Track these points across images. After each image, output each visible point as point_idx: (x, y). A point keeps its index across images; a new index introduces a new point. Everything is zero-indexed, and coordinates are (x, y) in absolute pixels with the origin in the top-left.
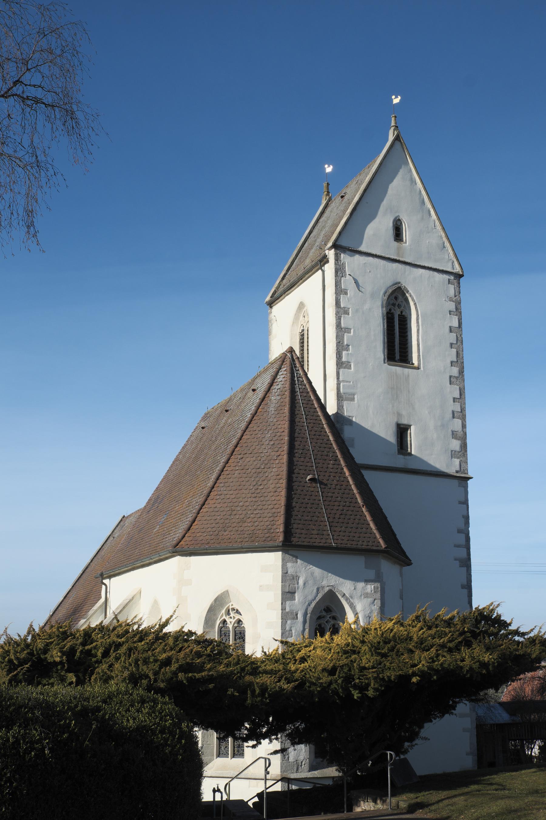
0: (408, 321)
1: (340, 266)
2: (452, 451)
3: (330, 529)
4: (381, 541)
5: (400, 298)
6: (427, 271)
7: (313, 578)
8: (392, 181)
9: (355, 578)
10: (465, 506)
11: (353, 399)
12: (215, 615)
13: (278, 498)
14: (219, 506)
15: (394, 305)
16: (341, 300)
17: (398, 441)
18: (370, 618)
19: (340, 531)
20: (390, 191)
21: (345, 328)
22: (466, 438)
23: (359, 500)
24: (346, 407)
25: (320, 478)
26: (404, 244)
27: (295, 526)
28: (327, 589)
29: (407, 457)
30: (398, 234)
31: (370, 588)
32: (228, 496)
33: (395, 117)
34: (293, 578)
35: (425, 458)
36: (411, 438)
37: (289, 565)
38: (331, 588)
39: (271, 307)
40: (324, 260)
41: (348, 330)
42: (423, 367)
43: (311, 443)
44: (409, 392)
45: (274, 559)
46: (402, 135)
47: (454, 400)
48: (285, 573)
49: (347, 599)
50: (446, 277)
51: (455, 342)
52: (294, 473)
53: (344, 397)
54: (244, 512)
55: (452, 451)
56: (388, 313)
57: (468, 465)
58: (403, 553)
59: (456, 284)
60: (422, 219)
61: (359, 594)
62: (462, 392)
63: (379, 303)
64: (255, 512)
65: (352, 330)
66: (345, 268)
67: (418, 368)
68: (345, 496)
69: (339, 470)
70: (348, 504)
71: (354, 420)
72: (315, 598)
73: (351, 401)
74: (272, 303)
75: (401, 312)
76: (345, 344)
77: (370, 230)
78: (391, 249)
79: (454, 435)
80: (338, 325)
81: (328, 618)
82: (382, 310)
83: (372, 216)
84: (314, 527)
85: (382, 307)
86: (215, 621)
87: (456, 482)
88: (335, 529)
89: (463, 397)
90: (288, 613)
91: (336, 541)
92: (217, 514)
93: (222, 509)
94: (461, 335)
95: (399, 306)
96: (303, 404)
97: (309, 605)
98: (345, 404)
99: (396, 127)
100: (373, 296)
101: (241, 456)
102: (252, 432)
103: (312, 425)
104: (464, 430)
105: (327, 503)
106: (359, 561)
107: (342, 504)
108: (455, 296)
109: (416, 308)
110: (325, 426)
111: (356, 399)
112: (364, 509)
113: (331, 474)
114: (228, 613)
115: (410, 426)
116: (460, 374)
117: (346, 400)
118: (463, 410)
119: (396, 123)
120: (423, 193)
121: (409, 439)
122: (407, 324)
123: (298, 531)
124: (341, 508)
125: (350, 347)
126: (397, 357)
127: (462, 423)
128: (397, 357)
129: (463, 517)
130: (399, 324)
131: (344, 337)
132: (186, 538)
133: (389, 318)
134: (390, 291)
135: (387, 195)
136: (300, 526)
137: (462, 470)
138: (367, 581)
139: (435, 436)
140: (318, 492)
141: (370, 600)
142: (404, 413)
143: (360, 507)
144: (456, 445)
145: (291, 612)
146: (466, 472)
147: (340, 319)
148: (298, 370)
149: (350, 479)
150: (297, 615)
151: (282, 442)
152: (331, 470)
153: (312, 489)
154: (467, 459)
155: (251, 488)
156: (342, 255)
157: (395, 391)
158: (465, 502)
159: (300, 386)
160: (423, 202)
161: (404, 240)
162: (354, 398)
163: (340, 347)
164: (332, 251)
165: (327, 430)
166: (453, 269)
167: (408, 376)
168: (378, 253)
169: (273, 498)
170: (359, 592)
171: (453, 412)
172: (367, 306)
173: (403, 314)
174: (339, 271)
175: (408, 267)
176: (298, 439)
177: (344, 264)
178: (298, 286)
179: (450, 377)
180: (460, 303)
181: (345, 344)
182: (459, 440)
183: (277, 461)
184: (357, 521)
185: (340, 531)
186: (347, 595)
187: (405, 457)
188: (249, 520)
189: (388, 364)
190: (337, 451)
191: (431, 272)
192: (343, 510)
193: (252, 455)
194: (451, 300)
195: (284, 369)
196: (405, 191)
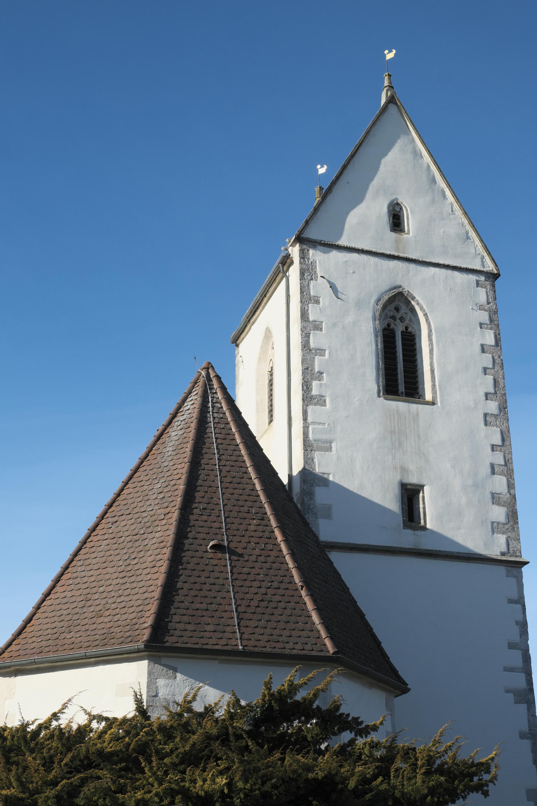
0: (417, 340)
1: (307, 265)
2: (493, 523)
3: (238, 624)
4: (328, 643)
5: (404, 309)
6: (443, 271)
8: (385, 154)
10: (519, 606)
11: (330, 449)
13: (155, 576)
14: (69, 594)
15: (393, 318)
16: (310, 311)
17: (403, 508)
19: (257, 627)
20: (382, 168)
21: (316, 350)
23: (297, 579)
24: (318, 460)
25: (232, 545)
26: (405, 236)
27: (176, 618)
29: (419, 533)
30: (396, 222)
32: (85, 580)
33: (389, 75)
36: (424, 503)
37: (161, 682)
39: (237, 346)
40: (286, 261)
41: (320, 352)
42: (442, 402)
43: (223, 494)
44: (419, 437)
46: (399, 97)
47: (493, 448)
50: (473, 278)
51: (491, 366)
53: (315, 445)
54: (104, 601)
55: (493, 523)
56: (384, 330)
57: (522, 544)
59: (488, 287)
60: (433, 201)
62: (505, 437)
63: (369, 314)
64: (119, 600)
65: (327, 352)
66: (316, 266)
67: (433, 403)
68: (272, 572)
69: (267, 534)
70: (275, 584)
71: (331, 478)
73: (327, 451)
74: (237, 339)
75: (407, 328)
76: (316, 371)
77: (353, 218)
78: (388, 242)
79: (495, 499)
80: (305, 345)
82: (374, 324)
83: (358, 199)
84: (209, 620)
85: (374, 319)
87: (502, 570)
88: (248, 623)
89: (507, 443)
91: (245, 643)
92: (65, 607)
93: (73, 599)
94: (499, 357)
95: (402, 319)
96: (216, 438)
98: (317, 456)
99: (391, 87)
100: (359, 304)
101: (115, 519)
102: (136, 484)
103: (228, 468)
104: (512, 491)
105: (238, 583)
110: (250, 470)
111: (334, 449)
112: (303, 593)
113: (252, 539)
115: (422, 486)
116: (500, 410)
117: (318, 451)
118: (508, 462)
119: (390, 83)
120: (433, 168)
121: (421, 506)
122: (415, 344)
123: (181, 626)
124: (263, 590)
125: (324, 375)
126: (402, 388)
128: (402, 388)
129: (517, 623)
130: (403, 344)
131: (313, 361)
132: (13, 648)
133: (387, 337)
134: (386, 297)
135: (379, 173)
136: (186, 619)
137: (511, 551)
139: (464, 500)
140: (226, 566)
142: (412, 467)
143: (297, 590)
144: (499, 514)
146: (518, 554)
147: (308, 337)
148: (216, 393)
149: (283, 547)
151: (176, 493)
152: (253, 534)
153: (214, 562)
154: (519, 535)
155: (121, 564)
156: (311, 252)
157: (396, 436)
158: (520, 601)
159: (216, 415)
160: (433, 181)
161: (406, 230)
162: (331, 448)
163: (309, 375)
164: (297, 247)
165: (253, 475)
166: (484, 267)
167: (418, 414)
168: (366, 248)
169: (149, 577)
171: (492, 466)
172: (350, 319)
173: (409, 330)
174: (308, 273)
175: (412, 266)
176: (202, 488)
177: (313, 264)
178: (264, 307)
179: (485, 415)
180: (496, 312)
181: (316, 371)
182: (503, 506)
183: (164, 522)
184: (288, 612)
185: (257, 627)
187: (416, 532)
188: (108, 613)
189: (385, 399)
190: (266, 506)
191: (449, 272)
192: (266, 594)
193: (130, 517)
195: (195, 393)
196: (404, 167)
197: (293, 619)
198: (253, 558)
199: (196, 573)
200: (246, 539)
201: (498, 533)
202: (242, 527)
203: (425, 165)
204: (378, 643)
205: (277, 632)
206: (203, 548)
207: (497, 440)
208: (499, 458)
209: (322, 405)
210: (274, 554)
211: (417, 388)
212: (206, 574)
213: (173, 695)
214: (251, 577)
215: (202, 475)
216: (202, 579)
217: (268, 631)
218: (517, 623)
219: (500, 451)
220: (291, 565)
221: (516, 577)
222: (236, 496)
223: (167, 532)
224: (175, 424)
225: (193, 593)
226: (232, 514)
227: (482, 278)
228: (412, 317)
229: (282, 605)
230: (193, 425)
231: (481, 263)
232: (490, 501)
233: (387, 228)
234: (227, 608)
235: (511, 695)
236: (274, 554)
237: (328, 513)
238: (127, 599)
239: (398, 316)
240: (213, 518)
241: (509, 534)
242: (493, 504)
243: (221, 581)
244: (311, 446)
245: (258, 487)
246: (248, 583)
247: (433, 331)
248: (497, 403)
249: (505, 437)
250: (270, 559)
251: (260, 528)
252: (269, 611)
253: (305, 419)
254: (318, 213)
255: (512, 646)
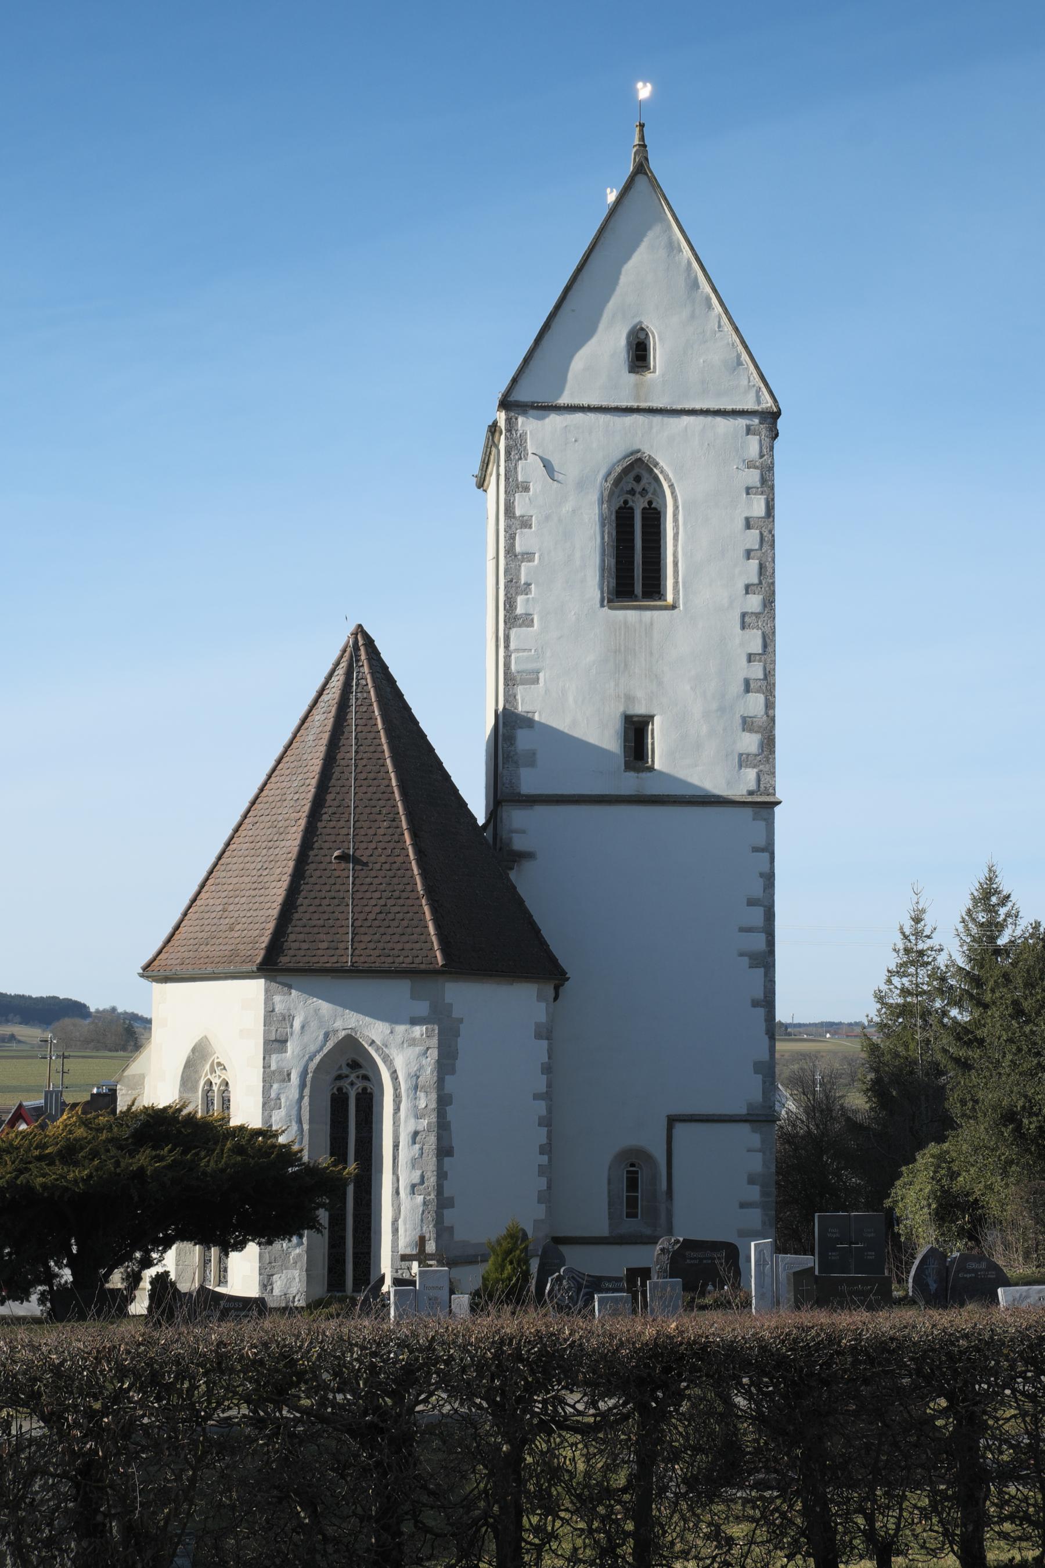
2: (741, 755)
6: (701, 419)
7: (320, 1018)
8: (627, 257)
9: (392, 1018)
10: (766, 855)
11: (536, 681)
12: (196, 1072)
15: (632, 492)
16: (516, 503)
18: (418, 1077)
20: (623, 279)
21: (523, 554)
22: (773, 727)
23: (419, 887)
25: (358, 854)
27: (292, 937)
28: (342, 1034)
29: (644, 775)
30: (639, 354)
31: (418, 1031)
34: (285, 1019)
35: (682, 774)
36: (653, 738)
37: (277, 998)
38: (349, 1032)
41: (528, 556)
42: (685, 604)
44: (651, 653)
45: (255, 988)
47: (750, 658)
48: (269, 1011)
49: (377, 1049)
50: (742, 422)
52: (313, 849)
53: (518, 678)
55: (741, 755)
57: (777, 778)
58: (553, 960)
59: (764, 432)
60: (693, 316)
61: (400, 1041)
63: (594, 496)
65: (537, 556)
67: (674, 607)
68: (395, 880)
69: (396, 837)
70: (396, 894)
71: (537, 718)
72: (321, 1049)
75: (650, 503)
77: (578, 363)
79: (747, 724)
81: (353, 1077)
83: (588, 332)
86: (197, 1081)
87: (748, 812)
89: (770, 649)
90: (274, 1072)
95: (644, 491)
96: (356, 725)
97: (311, 1059)
98: (520, 691)
100: (581, 485)
103: (364, 762)
104: (770, 712)
105: (359, 895)
106: (402, 988)
107: (388, 894)
108: (762, 456)
109: (673, 493)
110: (388, 761)
111: (541, 680)
112: (424, 902)
114: (213, 1071)
115: (652, 717)
116: (765, 606)
118: (769, 675)
121: (650, 741)
126: (638, 589)
127: (767, 700)
128: (638, 589)
129: (761, 875)
131: (519, 571)
134: (619, 469)
136: (301, 937)
138: (414, 1022)
139: (704, 729)
141: (418, 1049)
142: (639, 694)
144: (750, 742)
145: (279, 1071)
146: (771, 791)
147: (514, 539)
150: (289, 1075)
153: (337, 873)
154: (774, 767)
156: (520, 420)
157: (620, 656)
158: (769, 849)
160: (695, 285)
162: (538, 679)
163: (514, 588)
166: (759, 403)
168: (595, 402)
170: (399, 1038)
171: (747, 683)
172: (567, 507)
175: (657, 419)
177: (523, 436)
179: (744, 615)
182: (756, 732)
184: (405, 923)
186: (378, 1042)
189: (610, 608)
194: (750, 465)
197: (409, 930)
198: (378, 866)
199: (318, 887)
200: (373, 845)
201: (746, 767)
202: (371, 832)
203: (685, 262)
204: (536, 931)
205: (390, 945)
206: (327, 859)
207: (756, 647)
208: (757, 671)
209: (528, 626)
210: (400, 859)
211: (659, 585)
212: (327, 887)
213: (289, 1010)
214: (373, 888)
215: (337, 770)
216: (323, 894)
217: (380, 945)
218: (761, 875)
219: (760, 661)
220: (416, 871)
221: (765, 820)
222: (369, 795)
223: (293, 843)
224: (320, 704)
225: (312, 909)
226: (364, 817)
227: (756, 421)
228: (657, 488)
229: (400, 916)
230: (334, 710)
231: (754, 399)
232: (740, 728)
233: (625, 368)
234: (343, 923)
235: (746, 959)
236: (400, 859)
237: (531, 759)
238: (255, 914)
239: (638, 489)
240: (342, 823)
241: (761, 767)
242: (744, 730)
243: (341, 894)
244: (513, 679)
245: (394, 783)
246: (368, 895)
247: (680, 508)
248: (761, 597)
249: (768, 641)
250: (395, 866)
251: (390, 831)
252: (386, 923)
253: (507, 647)
254: (531, 363)
255: (751, 902)
